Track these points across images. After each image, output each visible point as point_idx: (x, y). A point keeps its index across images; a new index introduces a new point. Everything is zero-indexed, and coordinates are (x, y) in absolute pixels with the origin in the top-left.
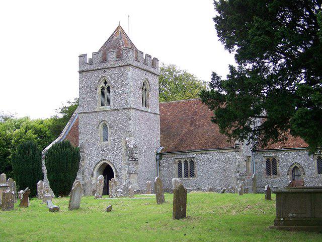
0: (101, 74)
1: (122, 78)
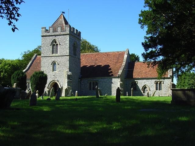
0: (54, 38)
1: (64, 40)
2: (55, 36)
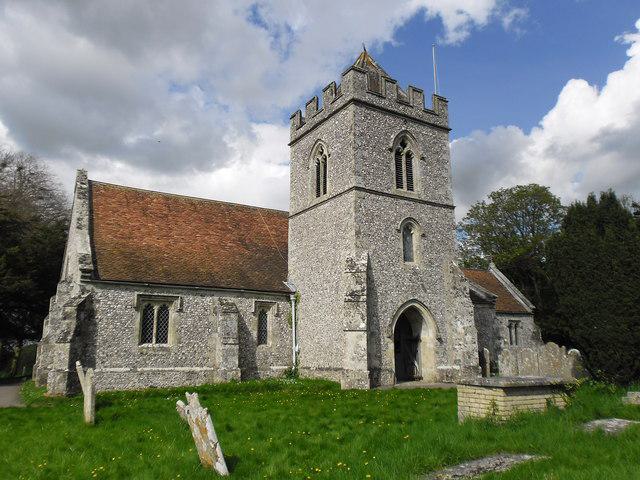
2: (407, 118)
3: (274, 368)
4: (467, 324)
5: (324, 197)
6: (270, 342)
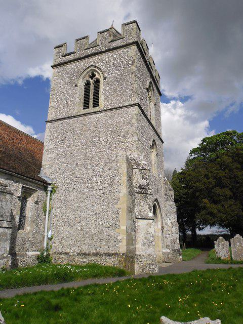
3: (30, 253)
4: (173, 220)
5: (97, 109)
6: (28, 228)
